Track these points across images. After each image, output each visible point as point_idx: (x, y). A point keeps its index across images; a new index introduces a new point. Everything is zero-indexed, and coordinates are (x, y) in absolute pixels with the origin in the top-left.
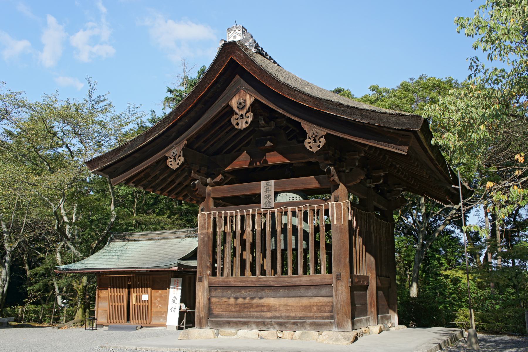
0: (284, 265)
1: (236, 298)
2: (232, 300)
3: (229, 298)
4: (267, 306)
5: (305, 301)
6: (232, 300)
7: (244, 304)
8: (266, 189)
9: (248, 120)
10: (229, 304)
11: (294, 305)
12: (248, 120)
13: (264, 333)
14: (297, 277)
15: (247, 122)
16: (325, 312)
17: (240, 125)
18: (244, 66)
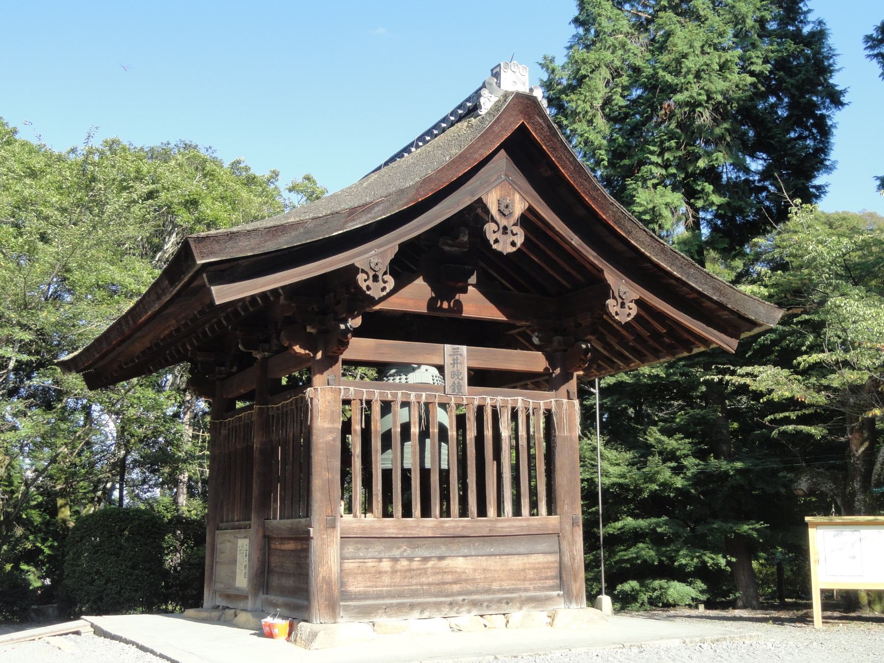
0: (445, 496)
1: (395, 560)
2: (386, 565)
3: (380, 560)
4: (452, 572)
5: (516, 562)
6: (386, 565)
7: (410, 570)
8: (454, 360)
9: (515, 238)
10: (380, 573)
11: (498, 568)
12: (515, 238)
13: (487, 620)
14: (520, 520)
15: (513, 244)
16: (547, 578)
17: (501, 243)
18: (547, 146)
